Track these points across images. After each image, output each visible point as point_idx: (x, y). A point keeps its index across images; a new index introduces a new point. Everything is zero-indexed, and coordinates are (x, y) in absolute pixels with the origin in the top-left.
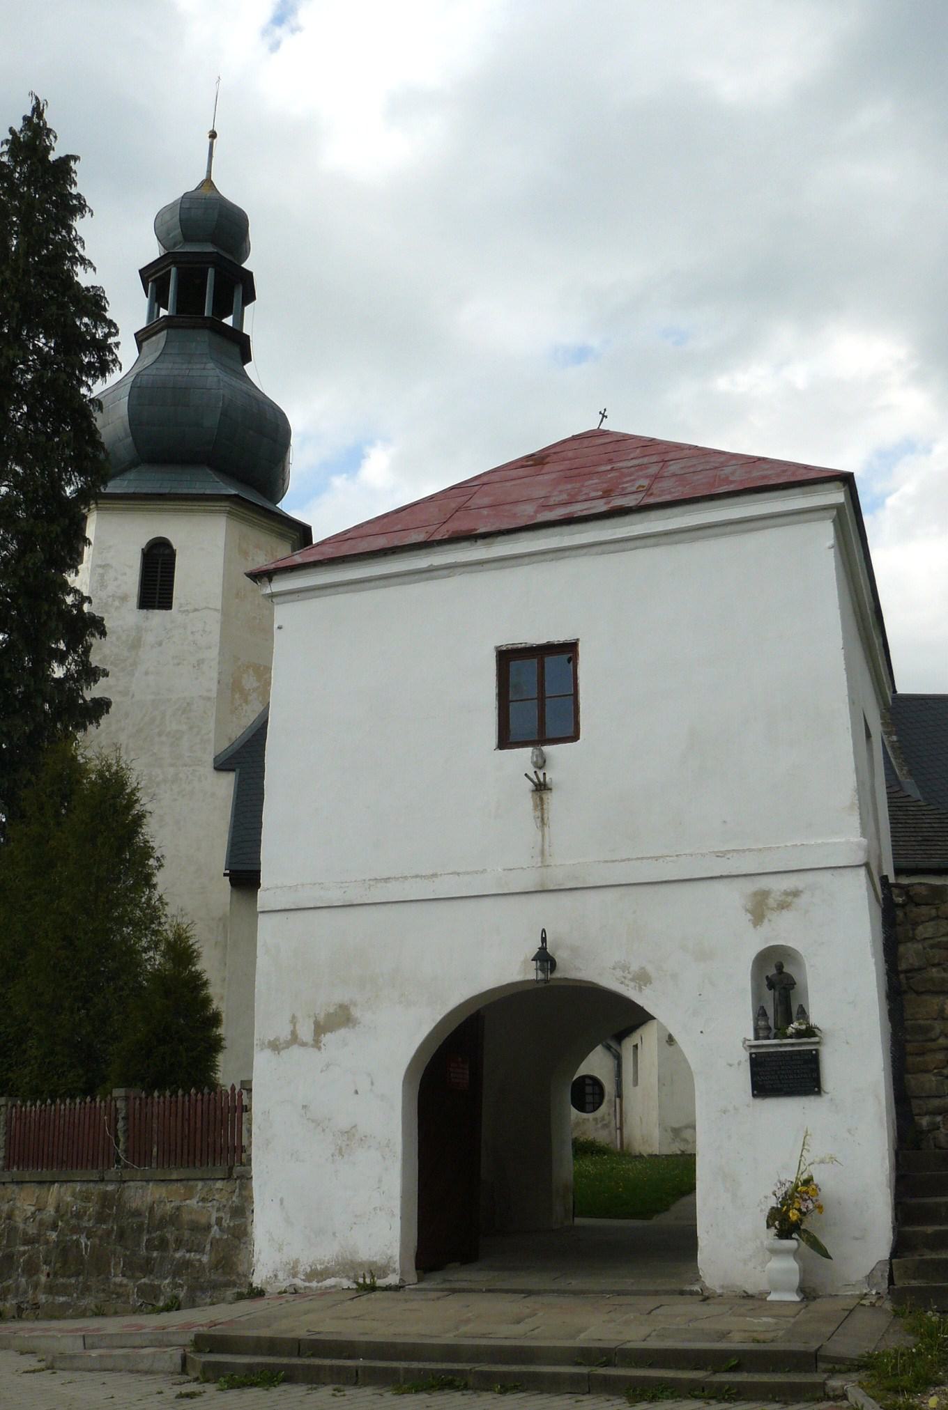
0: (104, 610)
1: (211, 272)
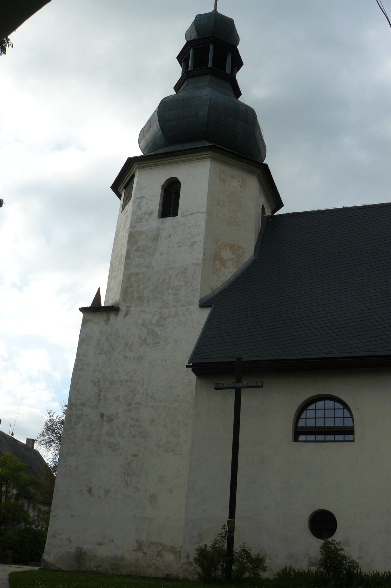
0: (139, 222)
1: (211, 47)
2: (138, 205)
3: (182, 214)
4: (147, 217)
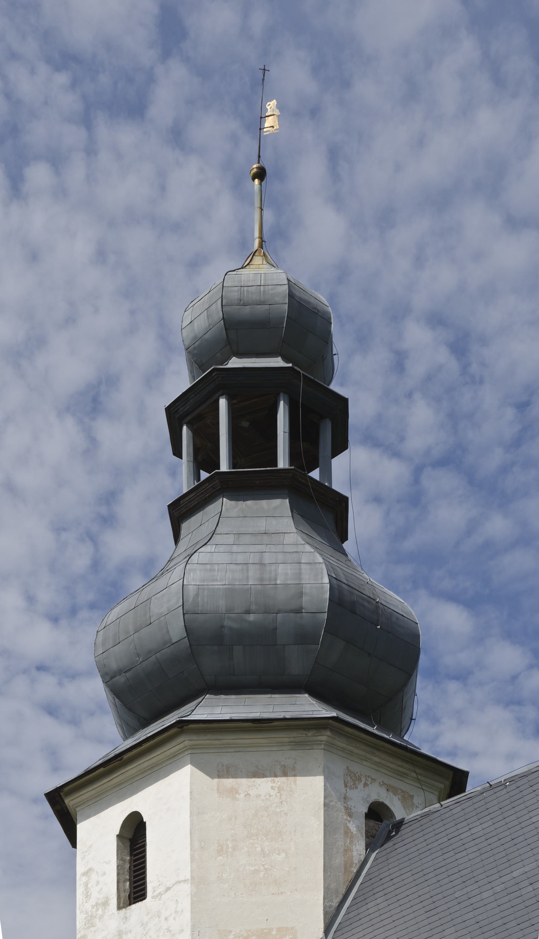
1: (223, 403)
2: (85, 889)
3: (153, 893)
4: (100, 912)
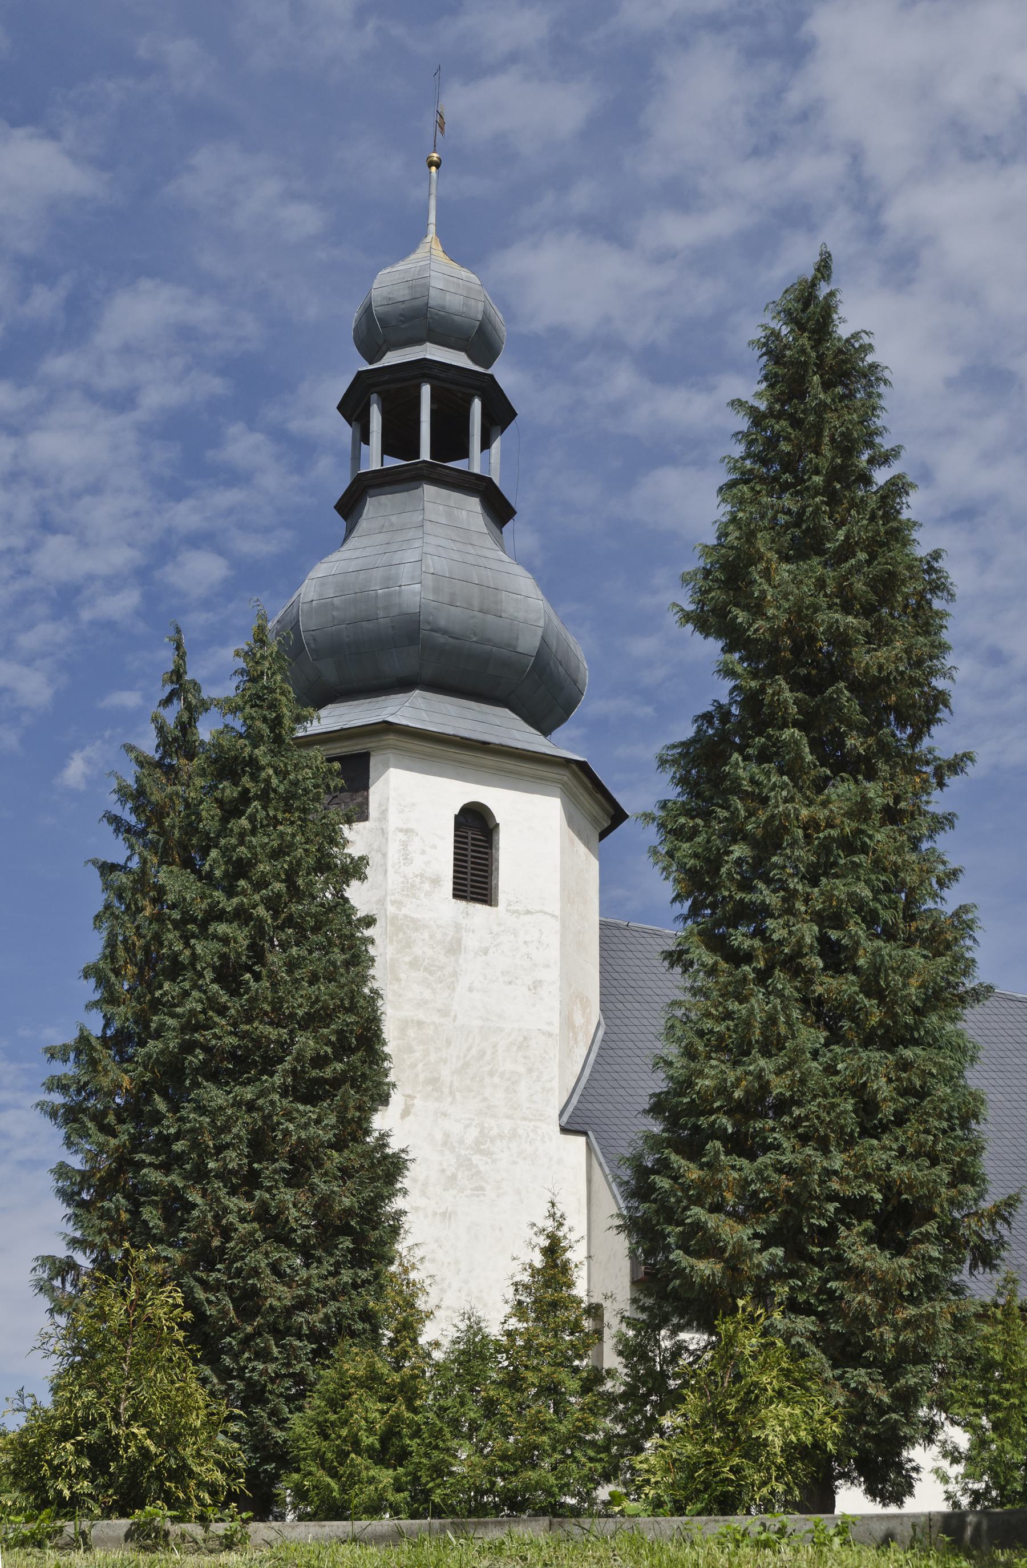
1: (426, 390)
